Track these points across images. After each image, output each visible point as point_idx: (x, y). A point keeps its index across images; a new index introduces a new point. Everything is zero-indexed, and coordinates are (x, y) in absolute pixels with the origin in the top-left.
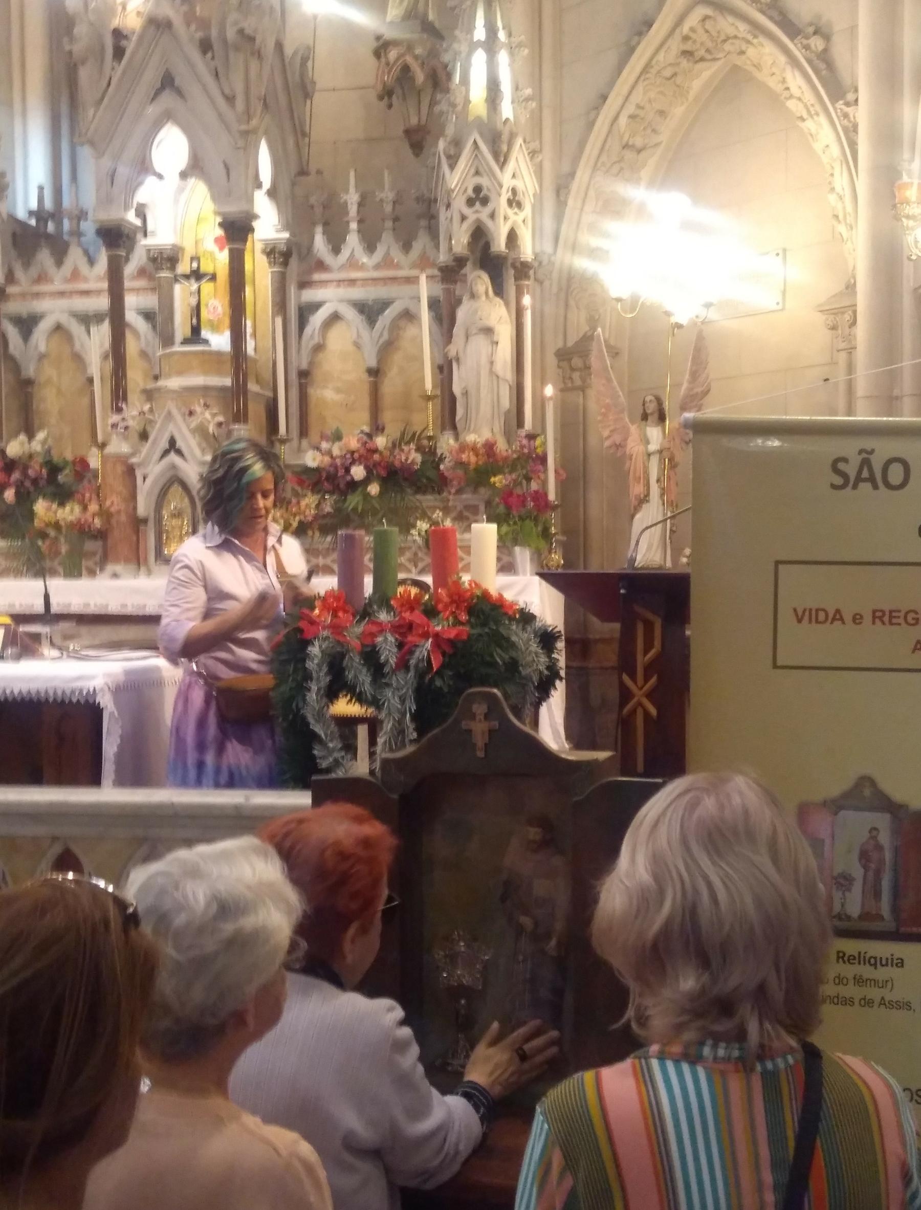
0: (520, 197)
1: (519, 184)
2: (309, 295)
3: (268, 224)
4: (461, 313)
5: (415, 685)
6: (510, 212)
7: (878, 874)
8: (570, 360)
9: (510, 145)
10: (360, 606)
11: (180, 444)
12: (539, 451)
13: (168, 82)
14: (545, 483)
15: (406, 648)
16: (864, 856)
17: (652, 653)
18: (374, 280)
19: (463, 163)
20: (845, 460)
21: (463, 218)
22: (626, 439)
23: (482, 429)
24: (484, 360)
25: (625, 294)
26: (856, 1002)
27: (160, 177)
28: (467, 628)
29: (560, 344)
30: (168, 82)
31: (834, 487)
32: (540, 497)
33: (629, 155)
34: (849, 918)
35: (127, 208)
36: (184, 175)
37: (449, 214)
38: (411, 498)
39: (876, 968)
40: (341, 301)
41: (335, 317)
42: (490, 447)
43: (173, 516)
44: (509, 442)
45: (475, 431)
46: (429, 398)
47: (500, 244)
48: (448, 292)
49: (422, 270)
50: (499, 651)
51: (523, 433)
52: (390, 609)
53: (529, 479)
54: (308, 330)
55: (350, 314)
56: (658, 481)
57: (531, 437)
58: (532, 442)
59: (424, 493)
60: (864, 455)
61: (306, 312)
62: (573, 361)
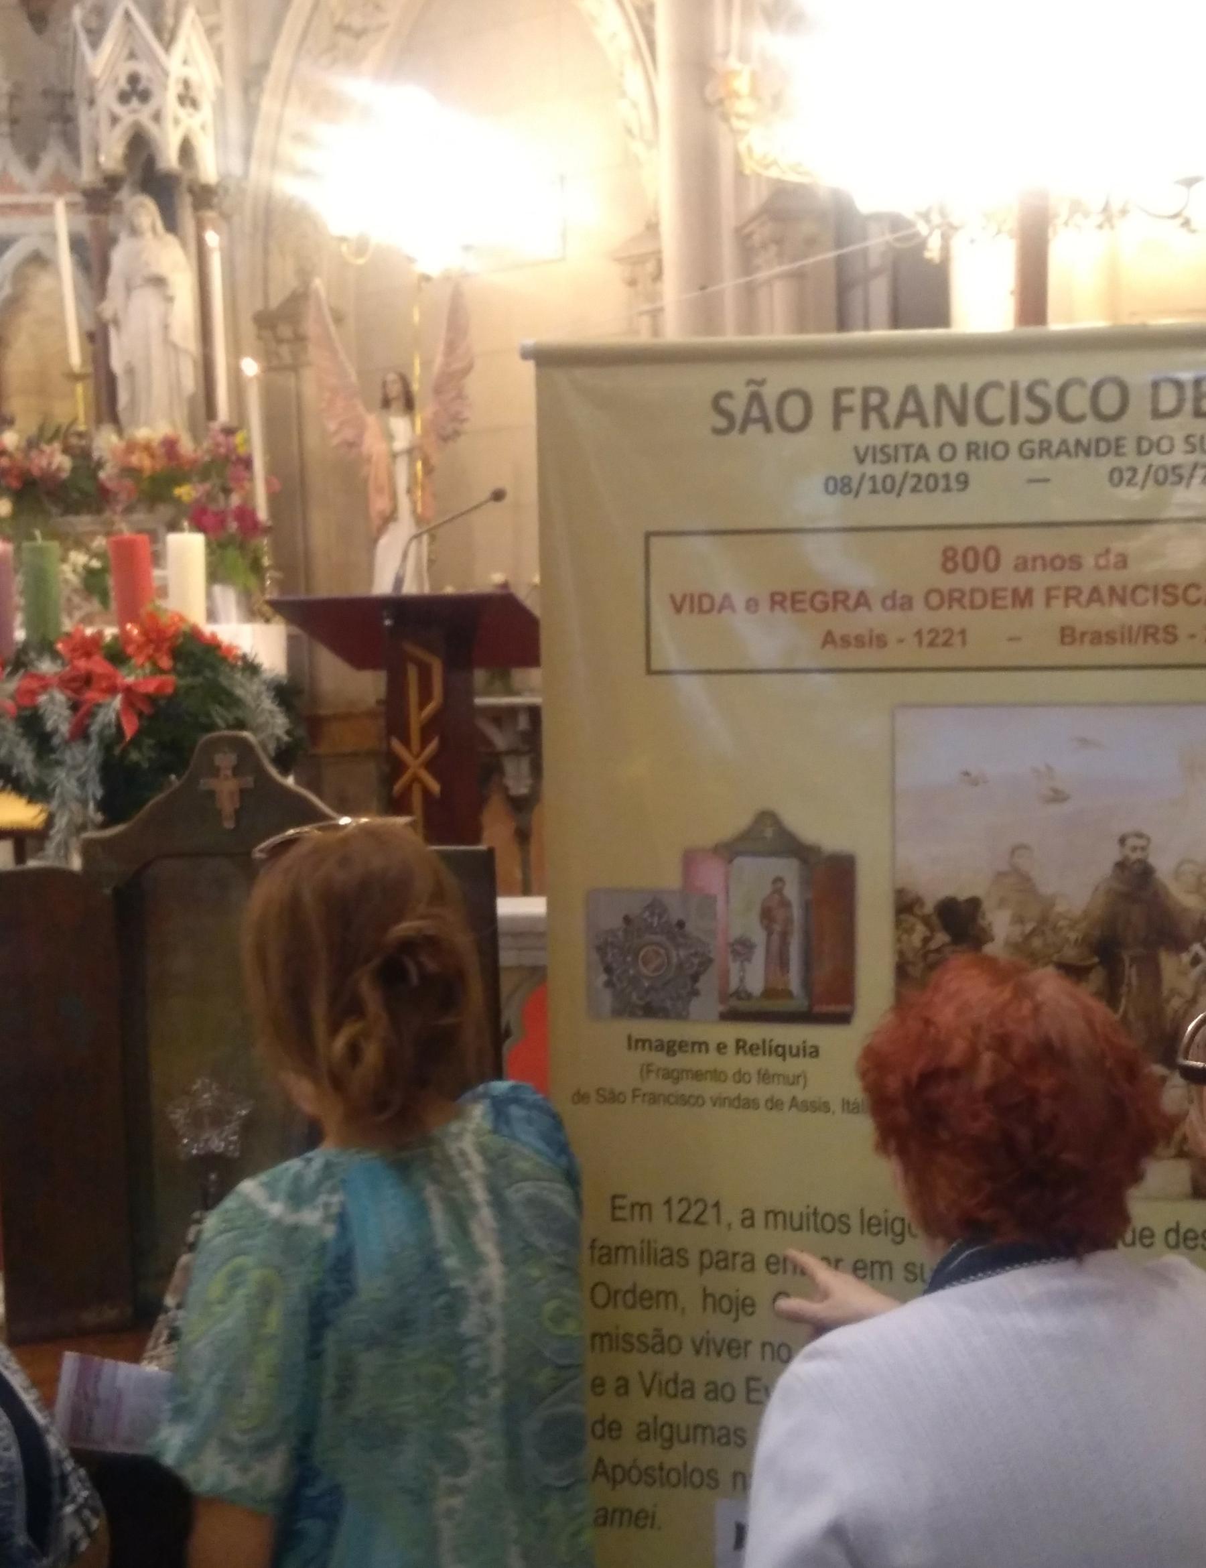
0: (195, 92)
1: (192, 73)
4: (119, 257)
5: (100, 760)
6: (182, 113)
7: (785, 936)
8: (273, 327)
9: (178, 16)
10: (10, 654)
12: (242, 451)
14: (249, 496)
15: (83, 709)
16: (767, 915)
17: (430, 708)
19: (108, 45)
20: (728, 395)
21: (115, 120)
22: (360, 435)
23: (156, 421)
24: (154, 323)
25: (352, 232)
26: (762, 1103)
28: (171, 678)
29: (259, 306)
31: (717, 431)
32: (245, 515)
33: (345, 40)
34: (749, 996)
37: (93, 113)
38: (60, 520)
39: (784, 1060)
42: (170, 445)
44: (196, 438)
45: (148, 423)
46: (75, 377)
47: (170, 158)
48: (95, 225)
49: (59, 192)
50: (218, 707)
51: (216, 426)
52: (55, 655)
53: (227, 491)
56: (409, 491)
57: (229, 431)
58: (231, 439)
59: (77, 512)
60: (753, 388)
62: (280, 326)
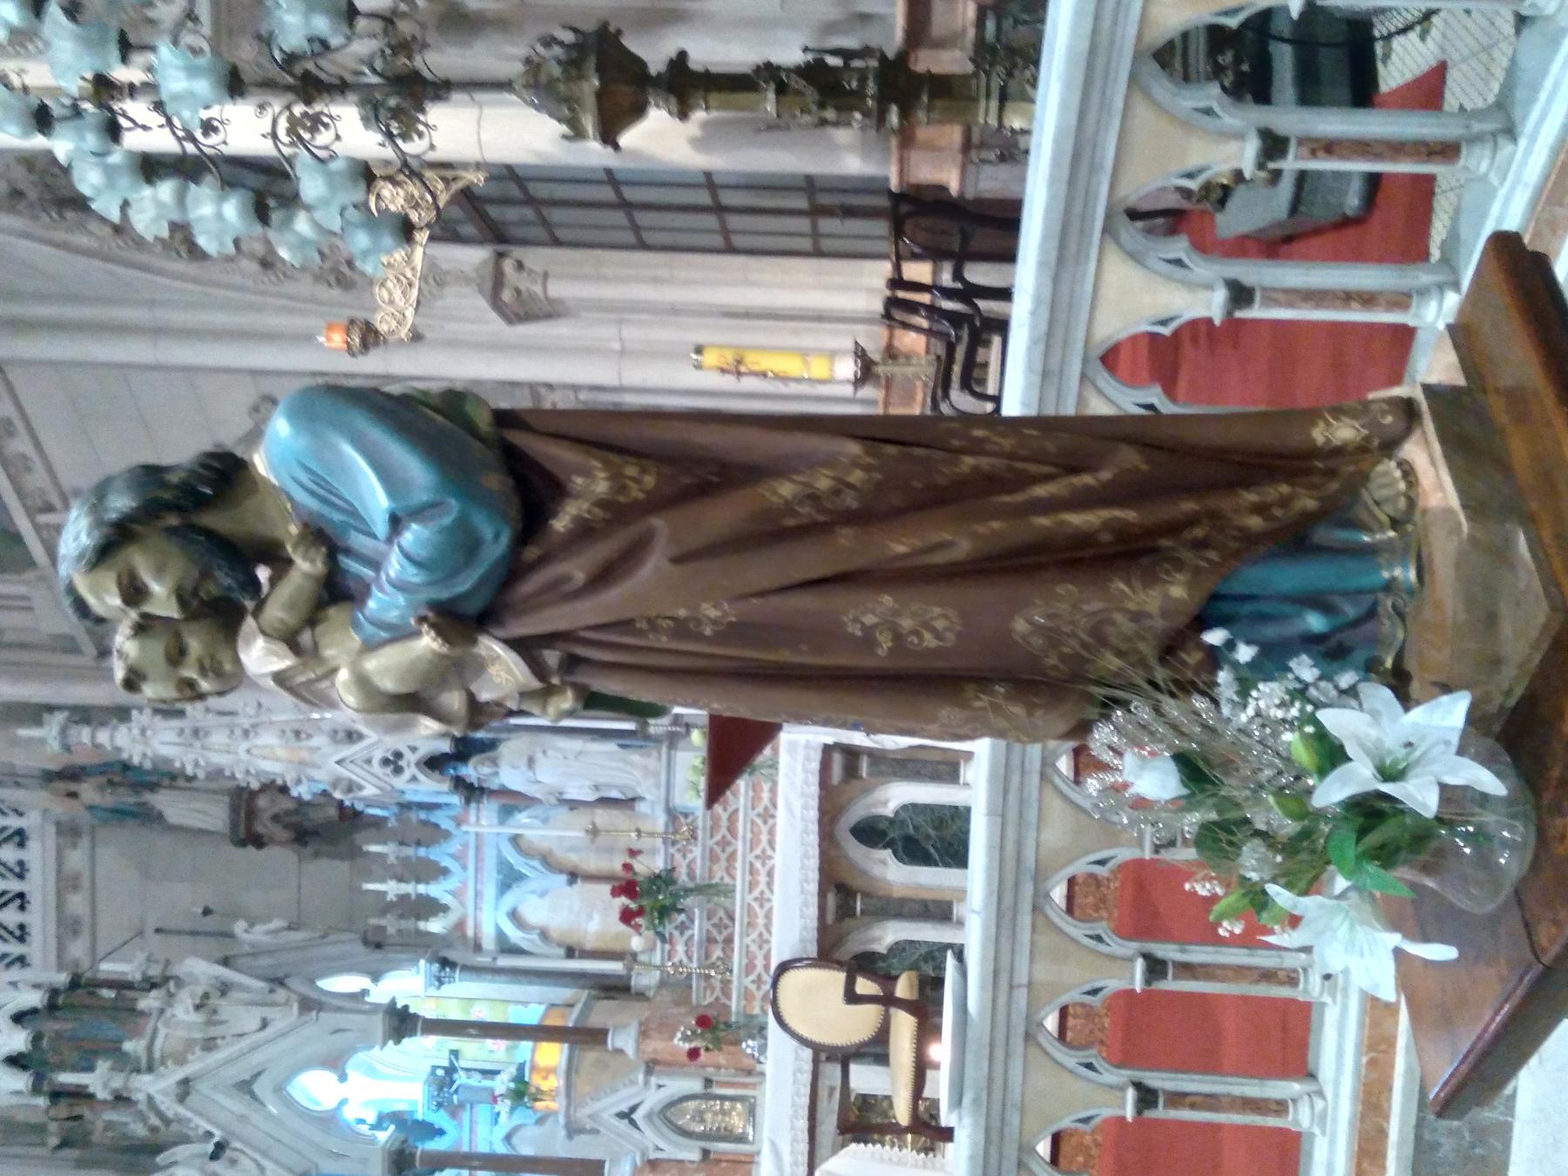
2: (489, 943)
3: (407, 985)
11: (624, 1107)
13: (245, 1087)
18: (477, 870)
27: (343, 1102)
30: (245, 1087)
35: (373, 1141)
36: (343, 1077)
40: (496, 908)
41: (514, 916)
43: (702, 1121)
54: (525, 946)
55: (509, 900)
61: (509, 949)
